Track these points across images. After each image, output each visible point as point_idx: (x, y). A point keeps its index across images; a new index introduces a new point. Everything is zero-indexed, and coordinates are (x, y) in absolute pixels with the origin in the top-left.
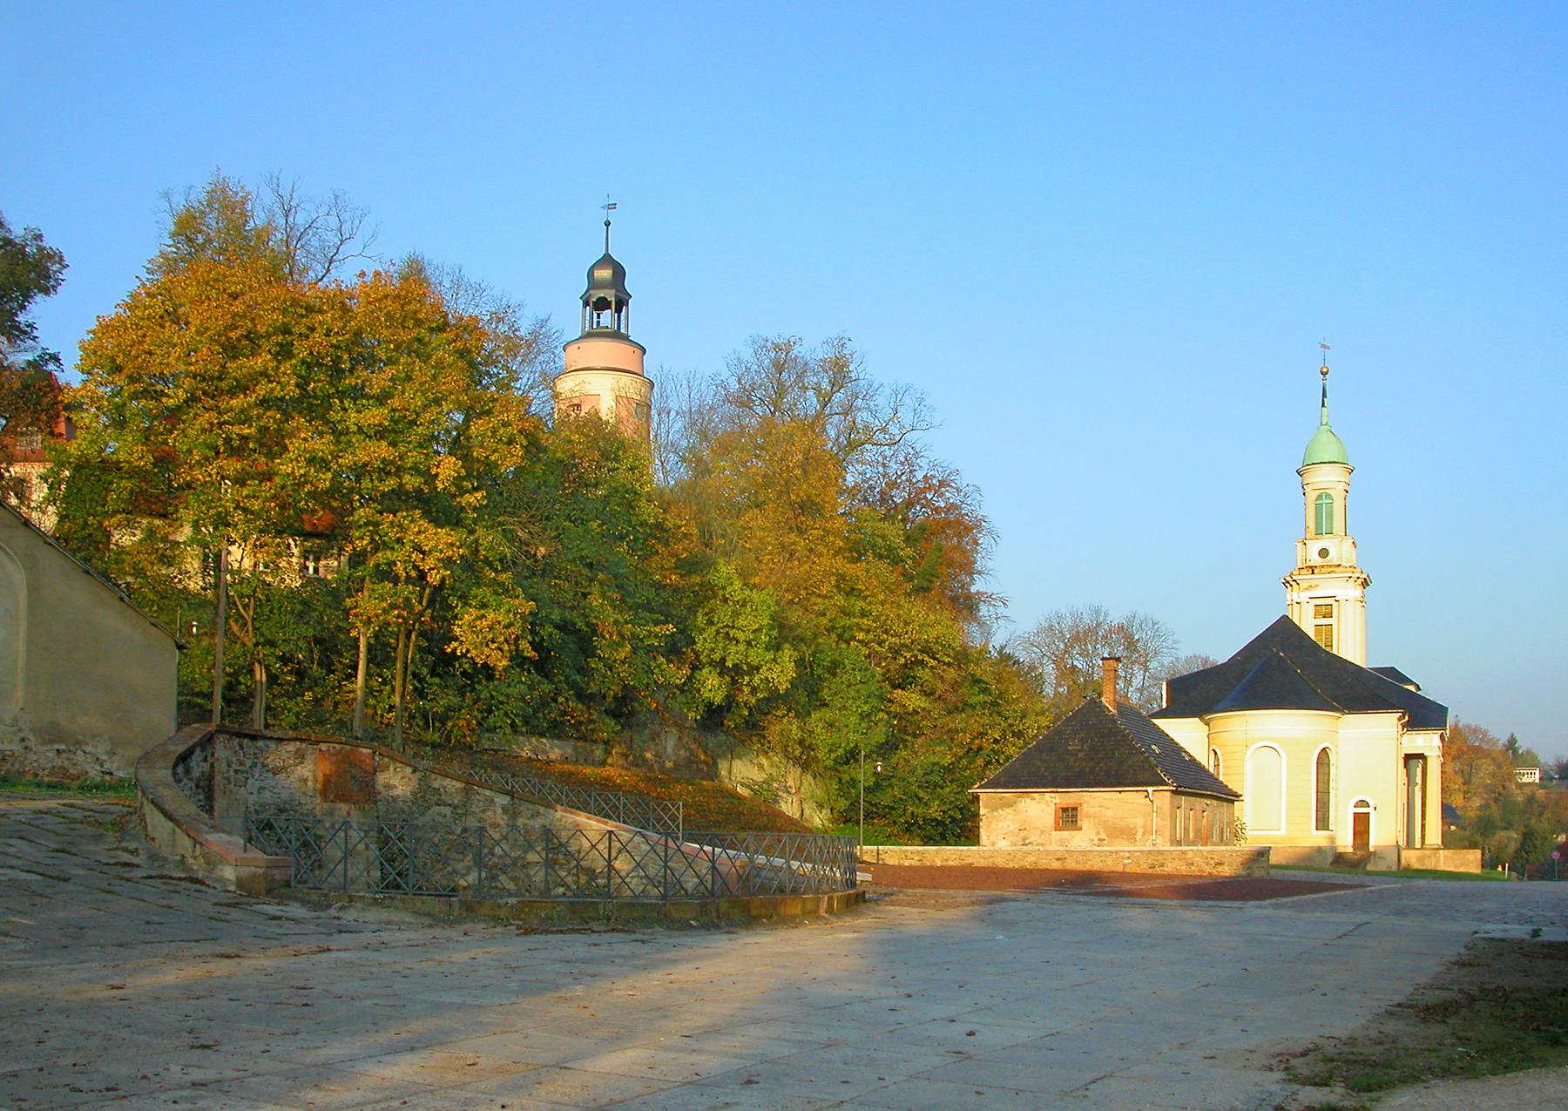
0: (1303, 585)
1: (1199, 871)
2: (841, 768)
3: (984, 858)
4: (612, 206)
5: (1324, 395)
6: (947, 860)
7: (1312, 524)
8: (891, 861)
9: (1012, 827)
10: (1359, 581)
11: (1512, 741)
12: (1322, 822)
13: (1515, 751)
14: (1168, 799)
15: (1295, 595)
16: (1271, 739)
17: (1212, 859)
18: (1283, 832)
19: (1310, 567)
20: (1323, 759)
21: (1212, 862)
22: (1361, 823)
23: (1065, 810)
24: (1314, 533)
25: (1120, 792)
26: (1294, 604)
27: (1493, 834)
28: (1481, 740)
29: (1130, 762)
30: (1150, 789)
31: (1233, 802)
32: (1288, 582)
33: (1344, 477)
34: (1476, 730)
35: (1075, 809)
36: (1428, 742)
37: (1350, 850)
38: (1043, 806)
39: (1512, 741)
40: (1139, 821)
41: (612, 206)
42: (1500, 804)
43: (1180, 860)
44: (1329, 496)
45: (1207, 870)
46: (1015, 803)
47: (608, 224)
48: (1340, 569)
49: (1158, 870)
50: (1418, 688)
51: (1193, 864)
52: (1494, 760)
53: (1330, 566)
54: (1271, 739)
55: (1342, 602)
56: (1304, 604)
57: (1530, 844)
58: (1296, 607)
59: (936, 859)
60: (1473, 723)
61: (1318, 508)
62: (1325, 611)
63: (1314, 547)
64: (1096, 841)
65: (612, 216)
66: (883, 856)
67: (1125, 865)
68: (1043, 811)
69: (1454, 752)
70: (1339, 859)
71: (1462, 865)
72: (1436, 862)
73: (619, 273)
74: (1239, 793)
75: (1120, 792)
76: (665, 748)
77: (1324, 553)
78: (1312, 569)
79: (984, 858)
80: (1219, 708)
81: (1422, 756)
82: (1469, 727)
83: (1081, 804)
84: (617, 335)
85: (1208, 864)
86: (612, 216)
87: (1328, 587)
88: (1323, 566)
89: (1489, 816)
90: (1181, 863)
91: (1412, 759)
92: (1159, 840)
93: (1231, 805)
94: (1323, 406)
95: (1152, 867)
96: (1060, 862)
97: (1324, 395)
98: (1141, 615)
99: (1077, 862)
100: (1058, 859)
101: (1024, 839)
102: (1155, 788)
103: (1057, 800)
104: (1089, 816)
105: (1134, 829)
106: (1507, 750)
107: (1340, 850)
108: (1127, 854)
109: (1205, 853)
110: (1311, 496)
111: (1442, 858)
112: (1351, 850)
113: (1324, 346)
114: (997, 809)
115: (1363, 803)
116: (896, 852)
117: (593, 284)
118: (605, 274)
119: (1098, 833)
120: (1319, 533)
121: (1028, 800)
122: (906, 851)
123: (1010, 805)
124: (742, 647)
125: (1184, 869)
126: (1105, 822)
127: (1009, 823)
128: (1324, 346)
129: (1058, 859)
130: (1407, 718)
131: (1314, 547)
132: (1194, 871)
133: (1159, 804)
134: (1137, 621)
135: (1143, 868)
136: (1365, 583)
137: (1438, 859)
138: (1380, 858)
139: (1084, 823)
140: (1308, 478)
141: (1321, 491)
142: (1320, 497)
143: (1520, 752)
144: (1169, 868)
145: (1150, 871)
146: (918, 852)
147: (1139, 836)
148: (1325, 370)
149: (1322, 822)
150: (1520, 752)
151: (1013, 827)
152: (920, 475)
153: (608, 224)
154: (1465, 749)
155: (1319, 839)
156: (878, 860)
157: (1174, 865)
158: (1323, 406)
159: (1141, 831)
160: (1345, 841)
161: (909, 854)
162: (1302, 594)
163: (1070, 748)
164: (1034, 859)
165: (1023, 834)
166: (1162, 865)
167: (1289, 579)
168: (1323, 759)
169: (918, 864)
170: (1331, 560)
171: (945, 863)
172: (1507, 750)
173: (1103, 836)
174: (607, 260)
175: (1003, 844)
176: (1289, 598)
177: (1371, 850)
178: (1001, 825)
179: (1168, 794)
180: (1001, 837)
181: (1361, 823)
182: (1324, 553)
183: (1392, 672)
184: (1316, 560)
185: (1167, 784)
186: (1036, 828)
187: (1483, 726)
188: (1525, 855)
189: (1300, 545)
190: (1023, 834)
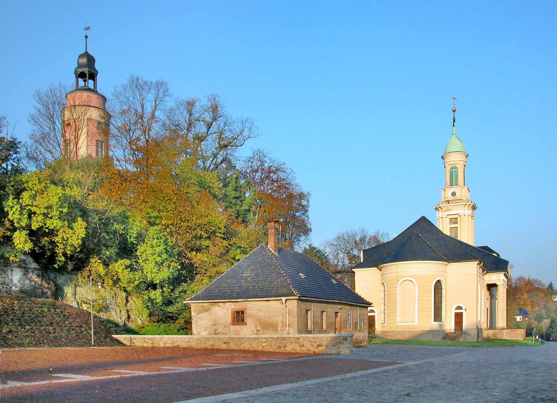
0: (444, 209)
1: (307, 350)
2: (143, 292)
3: (185, 342)
4: (88, 28)
5: (454, 121)
6: (166, 343)
7: (448, 182)
8: (138, 344)
9: (209, 324)
10: (470, 207)
11: (551, 285)
12: (438, 316)
13: (552, 288)
14: (296, 305)
15: (440, 214)
16: (409, 276)
17: (315, 342)
18: (416, 323)
19: (447, 201)
20: (438, 286)
21: (315, 344)
22: (459, 317)
23: (238, 312)
24: (449, 185)
25: (268, 301)
26: (440, 218)
27: (542, 321)
28: (539, 285)
29: (276, 283)
30: (284, 299)
31: (367, 307)
32: (437, 208)
33: (464, 158)
34: (536, 281)
35: (243, 312)
36: (497, 278)
37: (453, 331)
38: (225, 311)
39: (551, 285)
40: (279, 319)
41: (88, 28)
42: (546, 309)
43: (296, 343)
44: (456, 168)
45: (312, 349)
46: (210, 309)
47: (86, 37)
48: (461, 201)
49: (282, 350)
50: (498, 254)
51: (303, 346)
52: (543, 292)
53: (457, 200)
54: (409, 276)
55: (462, 216)
56: (444, 218)
57: (554, 325)
58: (441, 219)
59: (160, 343)
60: (535, 278)
61: (451, 173)
62: (454, 221)
63: (449, 192)
64: (255, 331)
65: (88, 33)
66: (134, 341)
67: (263, 346)
68: (225, 313)
69: (527, 290)
70: (447, 336)
71: (514, 336)
72: (502, 335)
73: (91, 60)
74: (371, 302)
75: (268, 301)
76: (12, 280)
77: (454, 194)
78: (448, 202)
79: (185, 342)
80: (385, 261)
81: (495, 285)
82: (534, 280)
83: (246, 309)
84: (94, 91)
85: (312, 346)
86: (88, 33)
87: (456, 210)
88: (453, 200)
89: (541, 314)
90: (297, 345)
91: (491, 287)
92: (291, 331)
93: (366, 309)
94: (454, 126)
95: (279, 347)
96: (226, 345)
97: (454, 121)
98: (381, 232)
99: (236, 345)
100: (225, 343)
101: (216, 330)
102: (287, 298)
103: (233, 307)
104: (251, 316)
105: (276, 323)
106: (549, 288)
107: (448, 331)
108: (264, 340)
109: (311, 339)
110: (448, 168)
111: (505, 334)
112: (453, 331)
113: (454, 98)
114: (200, 313)
115: (459, 308)
116: (139, 338)
117: (80, 66)
118: (84, 60)
119: (256, 327)
120: (451, 185)
121: (217, 307)
122: (145, 338)
123: (207, 310)
124: (41, 218)
125: (298, 349)
126: (260, 320)
127: (207, 321)
128: (454, 98)
129: (225, 343)
130: (482, 264)
131: (449, 192)
132: (304, 350)
133: (290, 308)
134: (380, 234)
135: (273, 348)
136: (474, 208)
137: (503, 334)
138: (469, 335)
139: (248, 320)
140: (446, 160)
141: (453, 165)
142: (452, 168)
143: (554, 289)
144: (290, 348)
145: (278, 350)
146: (151, 339)
147: (279, 328)
148: (454, 109)
149: (438, 316)
150: (554, 289)
151: (209, 323)
152: (266, 165)
153: (86, 37)
154: (532, 288)
155: (435, 325)
156: (131, 343)
157: (292, 346)
158: (454, 126)
159: (280, 325)
160: (449, 325)
161: (146, 340)
162: (444, 214)
163: (244, 275)
164: (211, 343)
165: (215, 327)
166: (285, 347)
167: (437, 207)
168: (438, 286)
169: (151, 345)
170: (457, 197)
171: (165, 345)
172: (549, 288)
173: (259, 328)
174: (86, 55)
175: (204, 334)
176: (438, 215)
177: (464, 331)
178: (202, 322)
179: (296, 301)
180: (203, 329)
181: (459, 317)
182: (454, 194)
183: (486, 248)
184: (450, 197)
185: (294, 295)
186: (221, 324)
187: (539, 279)
188: (551, 330)
189: (443, 191)
190: (215, 327)
